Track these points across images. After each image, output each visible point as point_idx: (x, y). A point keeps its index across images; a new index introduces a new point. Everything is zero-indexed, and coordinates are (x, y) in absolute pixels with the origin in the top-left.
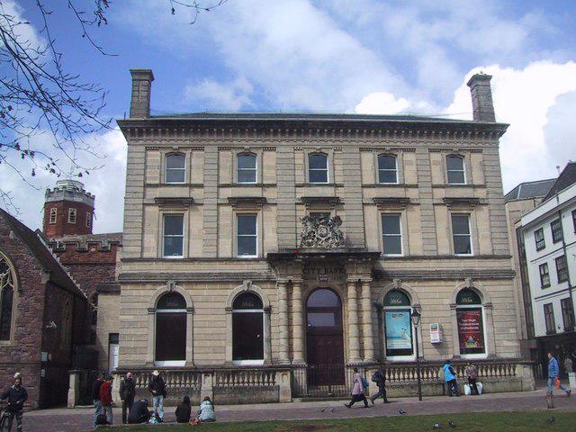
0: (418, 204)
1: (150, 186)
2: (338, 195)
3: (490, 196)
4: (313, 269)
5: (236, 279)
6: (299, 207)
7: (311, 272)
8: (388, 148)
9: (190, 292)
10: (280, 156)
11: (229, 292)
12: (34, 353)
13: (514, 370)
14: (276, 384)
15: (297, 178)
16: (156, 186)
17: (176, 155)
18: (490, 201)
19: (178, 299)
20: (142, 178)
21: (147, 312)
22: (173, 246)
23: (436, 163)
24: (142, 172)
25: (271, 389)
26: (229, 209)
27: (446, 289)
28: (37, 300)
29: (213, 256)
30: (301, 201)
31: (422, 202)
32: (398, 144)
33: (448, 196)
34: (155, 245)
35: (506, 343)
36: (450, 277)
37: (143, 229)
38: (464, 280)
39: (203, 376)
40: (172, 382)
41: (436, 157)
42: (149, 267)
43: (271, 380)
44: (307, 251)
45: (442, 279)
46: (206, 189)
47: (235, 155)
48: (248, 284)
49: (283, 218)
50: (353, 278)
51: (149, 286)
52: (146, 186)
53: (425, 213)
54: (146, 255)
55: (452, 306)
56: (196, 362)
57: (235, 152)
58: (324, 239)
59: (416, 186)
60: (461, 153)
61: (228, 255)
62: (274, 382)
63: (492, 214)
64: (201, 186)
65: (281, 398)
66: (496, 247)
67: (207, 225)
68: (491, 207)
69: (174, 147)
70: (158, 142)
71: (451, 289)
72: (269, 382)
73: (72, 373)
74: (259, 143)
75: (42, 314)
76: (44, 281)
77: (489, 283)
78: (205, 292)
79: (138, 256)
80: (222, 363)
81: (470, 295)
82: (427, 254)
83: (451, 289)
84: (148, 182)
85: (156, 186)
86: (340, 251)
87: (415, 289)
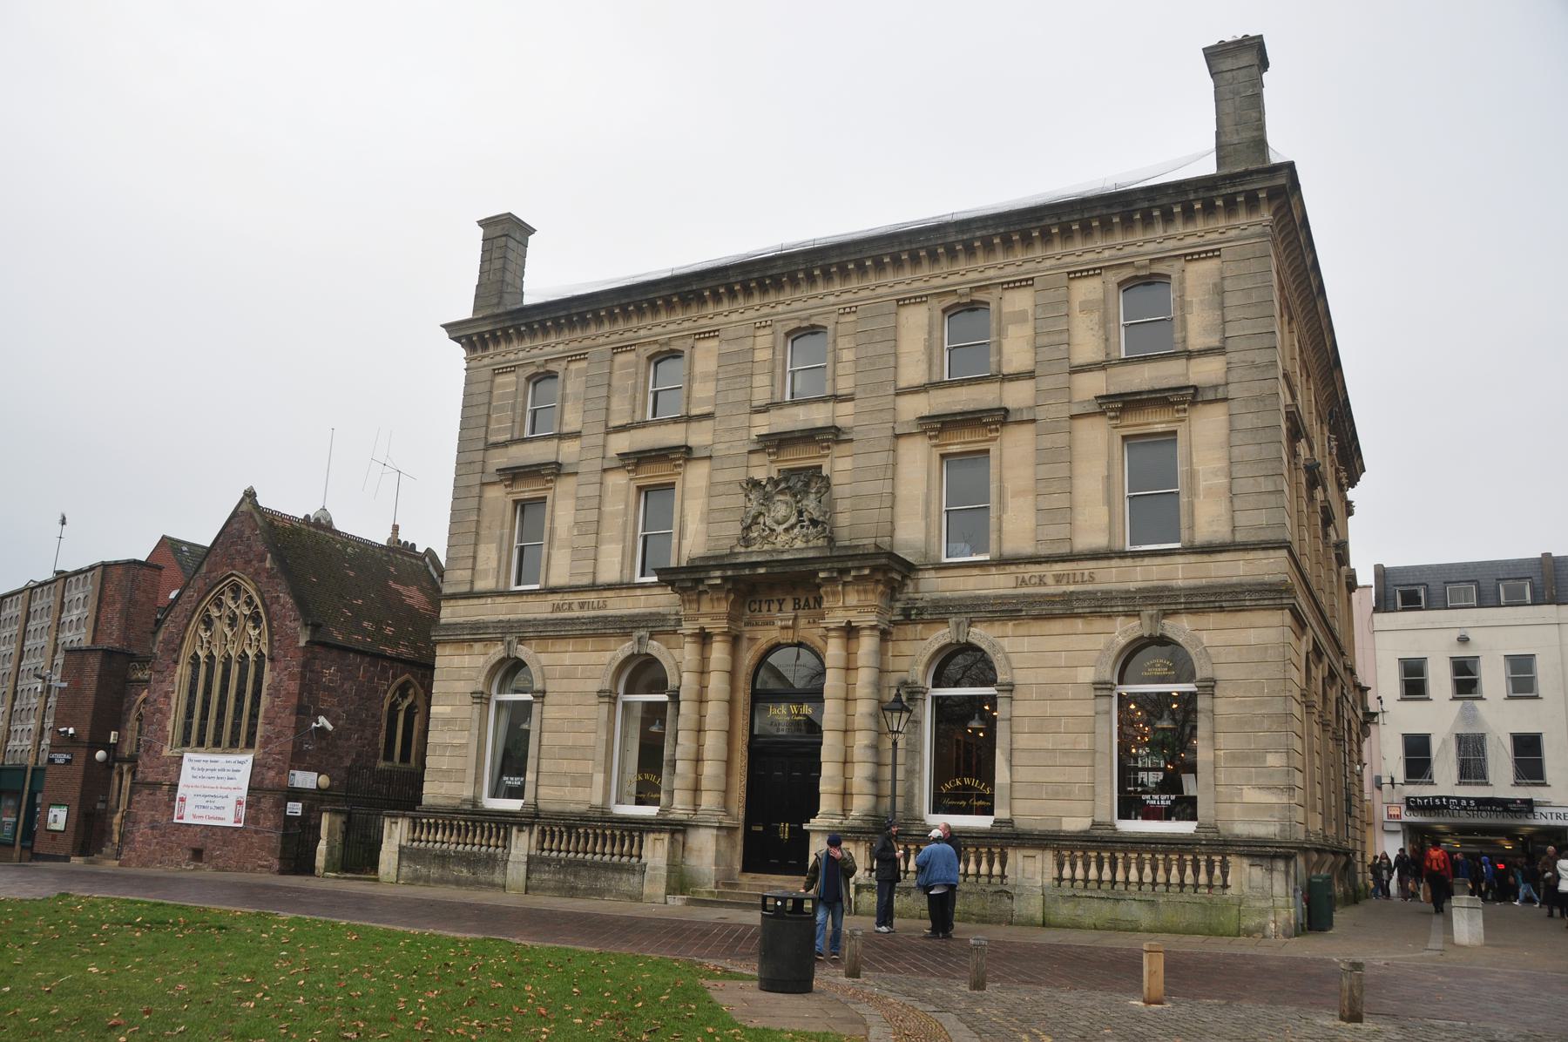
0: (1034, 421)
1: (496, 445)
2: (840, 423)
3: (1234, 377)
4: (769, 602)
5: (624, 626)
6: (755, 459)
7: (775, 607)
8: (964, 289)
9: (544, 658)
10: (726, 348)
11: (609, 655)
12: (281, 772)
13: (1003, 864)
14: (643, 860)
15: (756, 397)
16: (505, 444)
17: (1145, 281)
18: (1233, 391)
19: (976, 663)
20: (482, 433)
21: (469, 699)
22: (526, 562)
23: (1020, 317)
24: (484, 421)
25: (631, 870)
26: (619, 481)
27: (594, 657)
28: (292, 676)
29: (586, 580)
30: (496, 478)
31: (1041, 414)
32: (991, 273)
33: (1113, 391)
34: (494, 564)
35: (1252, 795)
36: (1101, 606)
37: (477, 534)
38: (1137, 615)
39: (514, 830)
40: (423, 837)
41: (1086, 290)
42: (630, 602)
43: (635, 851)
44: (741, 559)
45: (1078, 616)
46: (586, 441)
47: (1113, 286)
48: (640, 639)
49: (721, 489)
50: (837, 618)
51: (478, 647)
52: (900, 393)
53: (1047, 441)
54: (480, 585)
55: (1101, 687)
56: (541, 805)
57: (1113, 278)
58: (780, 529)
59: (1030, 375)
60: (978, 296)
61: (1099, 541)
62: (640, 857)
63: (1238, 425)
64: (576, 435)
65: (647, 890)
66: (1242, 519)
67: (582, 516)
68: (1235, 407)
69: (1139, 261)
70: (512, 357)
71: (1100, 642)
72: (560, 851)
73: (326, 811)
74: (686, 325)
75: (295, 701)
76: (302, 643)
77: (1212, 619)
78: (567, 659)
79: (465, 588)
80: (583, 808)
81: (511, 669)
82: (1044, 550)
83: (1100, 642)
84: (492, 439)
85: (505, 444)
86: (811, 554)
87: (1005, 643)
